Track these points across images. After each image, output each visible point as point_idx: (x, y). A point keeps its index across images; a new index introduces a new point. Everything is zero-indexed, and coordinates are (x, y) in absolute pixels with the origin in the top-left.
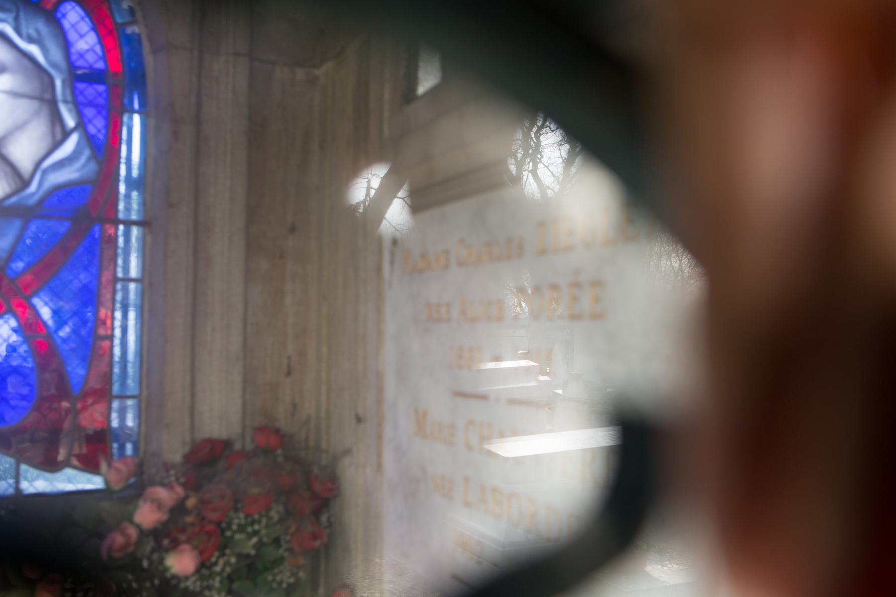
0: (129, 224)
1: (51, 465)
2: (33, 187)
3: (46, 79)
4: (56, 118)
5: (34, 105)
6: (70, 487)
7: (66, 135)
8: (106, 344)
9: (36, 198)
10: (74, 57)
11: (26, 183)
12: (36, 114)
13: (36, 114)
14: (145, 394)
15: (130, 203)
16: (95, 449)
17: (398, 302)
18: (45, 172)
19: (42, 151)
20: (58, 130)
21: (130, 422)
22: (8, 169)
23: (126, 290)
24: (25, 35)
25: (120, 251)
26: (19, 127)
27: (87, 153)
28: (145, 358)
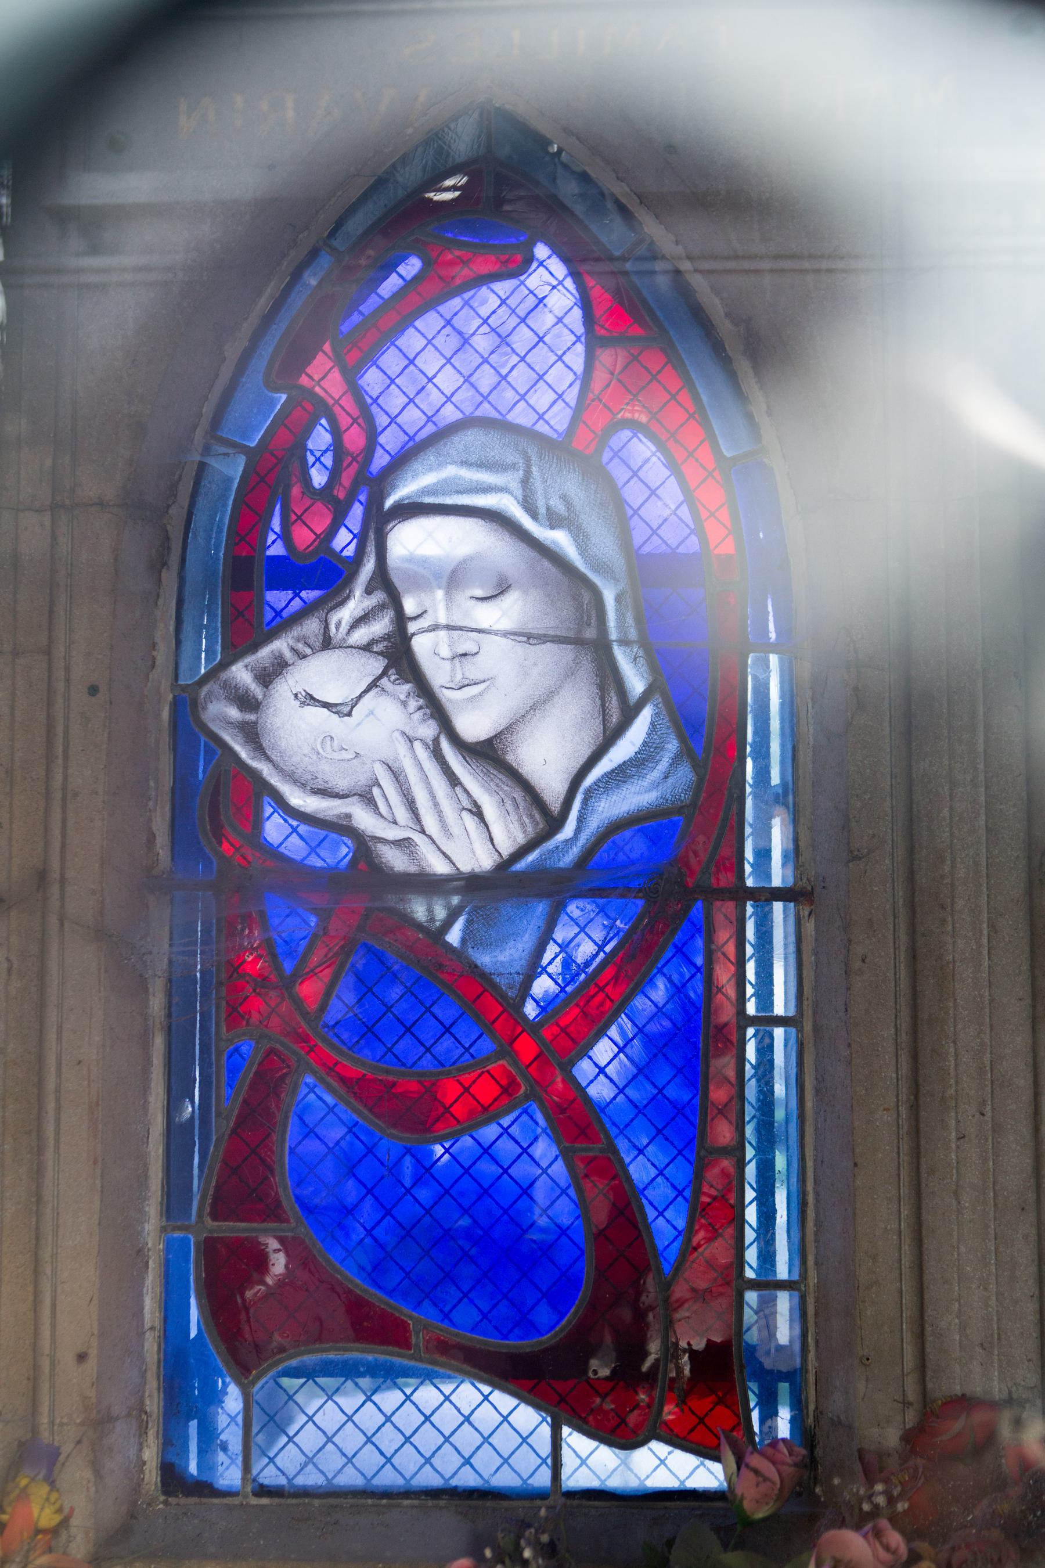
0: (767, 895)
1: (623, 1435)
2: (569, 829)
3: (586, 596)
4: (608, 677)
5: (566, 653)
6: (662, 1480)
7: (630, 713)
8: (727, 1163)
9: (575, 852)
10: (639, 535)
11: (554, 823)
12: (570, 673)
13: (570, 673)
14: (813, 1279)
15: (771, 847)
16: (707, 1399)
17: (428, 870)
18: (589, 794)
19: (585, 752)
20: (614, 702)
21: (784, 1333)
22: (518, 794)
23: (766, 1050)
24: (542, 510)
25: (750, 1235)
26: (537, 706)
27: (673, 746)
28: (811, 1198)
